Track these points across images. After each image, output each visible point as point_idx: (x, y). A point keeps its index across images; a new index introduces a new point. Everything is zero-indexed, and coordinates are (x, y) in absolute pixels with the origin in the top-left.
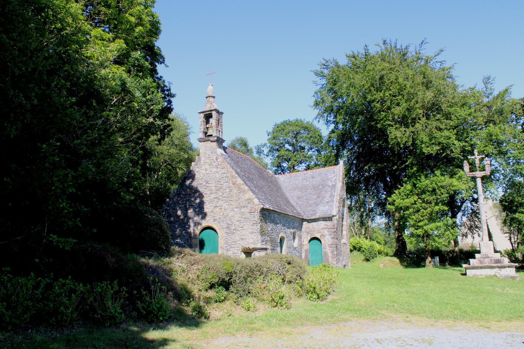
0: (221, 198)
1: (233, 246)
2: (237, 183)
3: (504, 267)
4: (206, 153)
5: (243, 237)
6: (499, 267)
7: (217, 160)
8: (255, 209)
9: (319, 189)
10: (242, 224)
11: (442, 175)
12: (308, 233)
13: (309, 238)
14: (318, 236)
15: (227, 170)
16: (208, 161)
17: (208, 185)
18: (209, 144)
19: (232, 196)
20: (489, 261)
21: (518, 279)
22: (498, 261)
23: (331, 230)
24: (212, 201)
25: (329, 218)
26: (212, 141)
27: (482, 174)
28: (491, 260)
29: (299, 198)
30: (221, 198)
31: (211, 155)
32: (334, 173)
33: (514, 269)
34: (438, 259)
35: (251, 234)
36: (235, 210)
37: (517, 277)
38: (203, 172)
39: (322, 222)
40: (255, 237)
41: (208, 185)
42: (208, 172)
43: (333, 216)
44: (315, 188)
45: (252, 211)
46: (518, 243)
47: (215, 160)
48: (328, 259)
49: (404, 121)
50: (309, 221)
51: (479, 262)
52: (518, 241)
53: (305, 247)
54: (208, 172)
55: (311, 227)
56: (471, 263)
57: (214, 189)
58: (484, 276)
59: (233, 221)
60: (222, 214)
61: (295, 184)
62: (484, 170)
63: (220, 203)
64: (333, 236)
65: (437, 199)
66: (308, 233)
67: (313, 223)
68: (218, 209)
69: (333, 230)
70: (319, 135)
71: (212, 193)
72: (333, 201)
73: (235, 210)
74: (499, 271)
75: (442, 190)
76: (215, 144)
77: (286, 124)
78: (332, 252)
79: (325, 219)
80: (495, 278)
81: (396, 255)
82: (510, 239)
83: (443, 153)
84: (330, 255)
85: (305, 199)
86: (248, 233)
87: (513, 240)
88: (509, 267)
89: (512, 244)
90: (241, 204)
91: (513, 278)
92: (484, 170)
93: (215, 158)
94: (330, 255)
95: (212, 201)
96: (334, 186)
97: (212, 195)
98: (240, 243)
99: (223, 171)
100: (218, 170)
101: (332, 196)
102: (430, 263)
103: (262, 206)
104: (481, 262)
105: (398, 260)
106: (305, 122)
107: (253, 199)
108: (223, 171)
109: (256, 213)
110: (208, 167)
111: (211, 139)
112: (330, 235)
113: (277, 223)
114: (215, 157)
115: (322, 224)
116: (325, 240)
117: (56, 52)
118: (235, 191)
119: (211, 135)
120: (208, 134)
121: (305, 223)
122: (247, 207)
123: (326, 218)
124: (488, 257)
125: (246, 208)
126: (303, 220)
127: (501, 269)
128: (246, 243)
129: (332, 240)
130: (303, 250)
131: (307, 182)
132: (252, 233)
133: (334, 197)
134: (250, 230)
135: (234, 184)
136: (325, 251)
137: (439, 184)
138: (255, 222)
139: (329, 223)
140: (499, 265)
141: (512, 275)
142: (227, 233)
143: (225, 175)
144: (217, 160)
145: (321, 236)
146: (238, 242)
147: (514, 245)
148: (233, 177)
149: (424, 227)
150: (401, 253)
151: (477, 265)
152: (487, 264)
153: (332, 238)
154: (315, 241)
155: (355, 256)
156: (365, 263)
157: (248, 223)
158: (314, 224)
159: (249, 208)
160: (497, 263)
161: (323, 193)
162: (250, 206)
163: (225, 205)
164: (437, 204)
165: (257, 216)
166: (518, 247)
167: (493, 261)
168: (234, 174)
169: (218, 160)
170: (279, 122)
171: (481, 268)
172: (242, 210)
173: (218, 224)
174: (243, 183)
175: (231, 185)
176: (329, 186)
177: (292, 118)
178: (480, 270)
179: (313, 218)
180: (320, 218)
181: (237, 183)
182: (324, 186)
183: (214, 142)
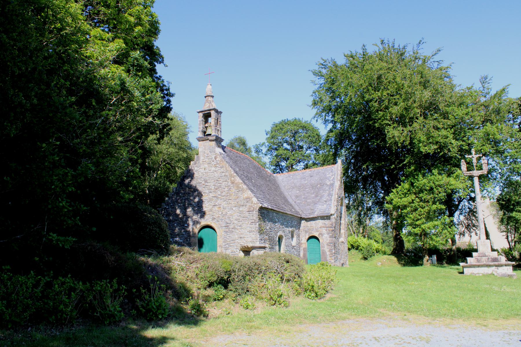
0: (220, 196)
1: (232, 245)
2: (236, 182)
3: (501, 266)
4: (205, 152)
5: (242, 236)
6: (496, 266)
7: (216, 159)
8: (254, 208)
9: (317, 188)
10: (241, 223)
11: (440, 174)
12: (306, 232)
13: (307, 237)
14: (316, 235)
15: (226, 169)
16: (207, 160)
17: (207, 184)
18: (207, 143)
19: (231, 195)
20: (486, 260)
21: (515, 278)
22: (495, 260)
23: (329, 229)
24: (210, 200)
25: (327, 216)
26: (210, 141)
27: (480, 173)
28: (488, 258)
29: (297, 197)
30: (220, 196)
31: (210, 154)
32: (332, 172)
33: (511, 268)
34: (435, 257)
35: (250, 232)
36: (234, 209)
37: (514, 275)
38: (202, 171)
39: (320, 221)
40: (253, 236)
41: (207, 184)
42: (207, 171)
43: (331, 215)
44: (313, 187)
45: (251, 210)
46: (515, 242)
47: (214, 159)
48: (326, 258)
49: (402, 120)
50: (308, 220)
51: (476, 260)
52: (515, 239)
53: (304, 246)
54: (207, 171)
55: (309, 225)
56: (468, 261)
57: (213, 188)
58: (481, 275)
59: (232, 219)
60: (220, 213)
61: (293, 183)
62: (482, 169)
63: (219, 201)
64: (331, 235)
65: (435, 198)
66: (306, 232)
67: (311, 222)
68: (216, 208)
69: (331, 229)
70: (317, 135)
71: (211, 192)
72: (331, 200)
73: (234, 209)
74: (496, 270)
75: (440, 189)
76: (214, 143)
77: (284, 123)
78: (330, 251)
79: (323, 218)
80: (492, 276)
81: (394, 253)
82: (507, 238)
83: (441, 152)
84: (328, 253)
85: (304, 198)
86: (246, 231)
87: (510, 239)
88: (506, 265)
89: (509, 243)
90: (240, 203)
91: (510, 276)
92: (482, 169)
93: (213, 157)
94: (328, 253)
95: (210, 200)
96: (332, 185)
97: (210, 194)
98: (239, 241)
99: (222, 170)
100: (217, 169)
101: (330, 195)
102: (427, 261)
103: (261, 205)
104: (478, 261)
105: (395, 259)
106: (304, 121)
107: (252, 197)
108: (222, 170)
109: (255, 212)
110: (206, 166)
111: (210, 138)
112: (328, 234)
113: (275, 222)
114: (214, 156)
115: (320, 222)
116: (323, 239)
117: (55, 52)
118: (233, 190)
119: (210, 135)
120: (207, 133)
121: (303, 222)
122: (246, 205)
123: (325, 216)
124: (486, 256)
125: (244, 207)
126: (301, 219)
127: (499, 268)
128: (245, 242)
129: (330, 239)
130: (302, 248)
131: (305, 181)
132: (250, 232)
133: (332, 196)
134: (249, 229)
135: (233, 183)
136: (323, 250)
137: (437, 183)
138: (253, 221)
139: (327, 222)
140: (496, 263)
141: (509, 274)
142: (226, 232)
143: (223, 174)
144: (216, 159)
145: (319, 235)
146: (237, 241)
147: (511, 244)
148: (231, 176)
149: (422, 226)
150: (399, 251)
151: (474, 263)
152: (485, 263)
153: (330, 237)
154: (314, 240)
155: (353, 255)
156: (363, 261)
157: (247, 222)
158: (313, 222)
159: (247, 206)
160: (494, 262)
161: (321, 192)
162: (249, 204)
163: (224, 204)
164: (434, 203)
165: (256, 214)
166: (515, 245)
167: (490, 260)
168: (232, 173)
169: (217, 159)
170: (277, 121)
171: (479, 266)
172: (241, 209)
173: (217, 223)
174: (241, 181)
175: (230, 183)
176: (328, 185)
177: (291, 118)
178: (477, 268)
179: (312, 216)
180: (318, 217)
181: (236, 182)
182: (322, 185)
183: (213, 141)
